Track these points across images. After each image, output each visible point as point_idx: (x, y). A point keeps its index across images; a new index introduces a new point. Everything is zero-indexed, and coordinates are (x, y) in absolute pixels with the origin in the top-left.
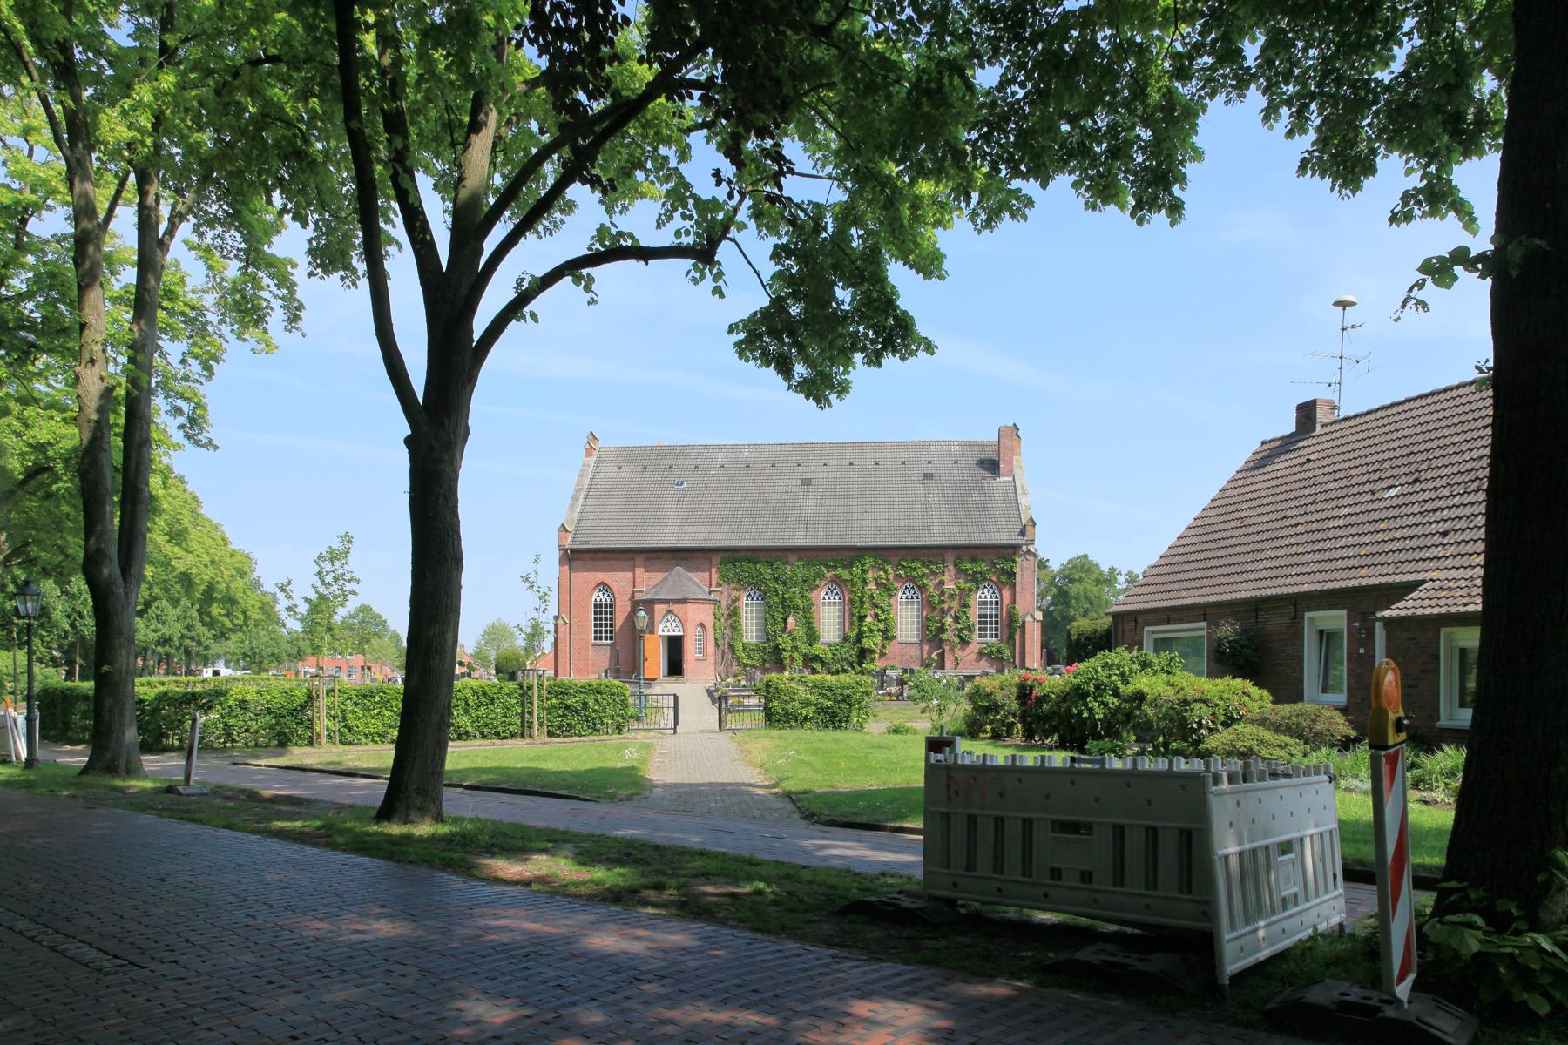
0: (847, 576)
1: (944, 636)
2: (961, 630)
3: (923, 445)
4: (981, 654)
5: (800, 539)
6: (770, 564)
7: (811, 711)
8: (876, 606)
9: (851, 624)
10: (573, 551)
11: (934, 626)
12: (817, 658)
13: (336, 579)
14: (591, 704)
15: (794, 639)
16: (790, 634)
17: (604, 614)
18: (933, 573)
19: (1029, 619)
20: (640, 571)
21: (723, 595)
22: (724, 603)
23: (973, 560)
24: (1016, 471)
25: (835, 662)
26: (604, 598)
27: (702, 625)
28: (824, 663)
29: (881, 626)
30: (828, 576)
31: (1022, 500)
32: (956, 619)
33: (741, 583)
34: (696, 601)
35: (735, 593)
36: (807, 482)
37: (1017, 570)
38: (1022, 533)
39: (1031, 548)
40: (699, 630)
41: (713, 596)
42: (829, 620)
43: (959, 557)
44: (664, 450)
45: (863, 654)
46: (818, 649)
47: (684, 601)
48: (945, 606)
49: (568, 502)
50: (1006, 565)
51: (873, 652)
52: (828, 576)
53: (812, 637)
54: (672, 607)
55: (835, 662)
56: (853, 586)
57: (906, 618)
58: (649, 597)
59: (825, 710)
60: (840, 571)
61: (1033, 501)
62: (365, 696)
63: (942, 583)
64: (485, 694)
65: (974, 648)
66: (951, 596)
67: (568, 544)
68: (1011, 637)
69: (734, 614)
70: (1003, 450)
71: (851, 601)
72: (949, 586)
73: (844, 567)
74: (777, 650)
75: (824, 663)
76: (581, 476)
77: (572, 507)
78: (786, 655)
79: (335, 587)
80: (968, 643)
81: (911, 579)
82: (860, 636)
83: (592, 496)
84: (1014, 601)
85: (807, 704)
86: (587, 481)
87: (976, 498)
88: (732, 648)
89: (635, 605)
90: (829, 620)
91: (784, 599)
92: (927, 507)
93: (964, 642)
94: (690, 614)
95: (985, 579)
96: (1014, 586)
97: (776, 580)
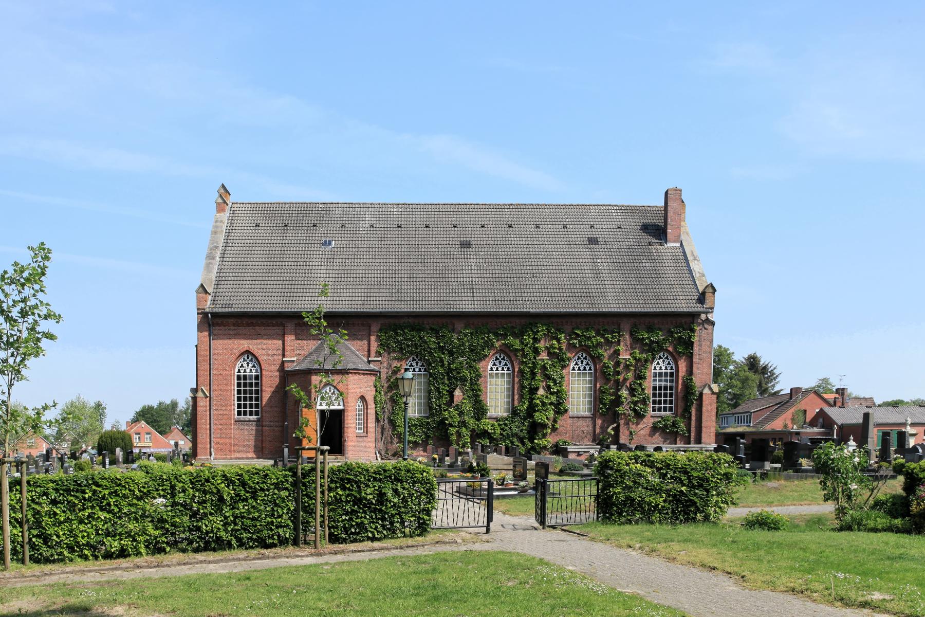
0: (517, 344)
1: (620, 409)
2: (635, 403)
3: (583, 208)
4: (655, 428)
5: (468, 304)
6: (435, 332)
7: (660, 500)
8: (548, 377)
9: (521, 397)
10: (215, 315)
11: (608, 398)
12: (485, 434)
13: (24, 314)
14: (390, 494)
15: (461, 414)
16: (457, 408)
17: (248, 388)
18: (608, 343)
19: (706, 391)
20: (290, 339)
21: (384, 365)
22: (384, 374)
23: (650, 329)
24: (683, 237)
25: (504, 438)
26: (250, 370)
27: (363, 398)
28: (492, 439)
29: (554, 399)
30: (497, 345)
31: (694, 266)
32: (632, 391)
33: (402, 352)
34: (357, 372)
35: (396, 364)
36: (466, 245)
37: (695, 339)
38: (702, 299)
39: (710, 316)
40: (360, 404)
41: (372, 366)
42: (497, 394)
43: (635, 326)
44: (305, 209)
45: (535, 429)
46: (487, 424)
47: (344, 372)
48: (621, 378)
49: (203, 262)
50: (684, 334)
51: (545, 426)
52: (497, 345)
53: (480, 410)
54: (331, 377)
55: (504, 438)
56: (524, 356)
57: (578, 391)
58: (303, 366)
59: (676, 498)
60: (510, 340)
61: (705, 269)
62: (68, 491)
63: (617, 353)
64: (244, 484)
65: (648, 422)
66: (627, 367)
67: (208, 306)
68: (687, 410)
69: (394, 385)
70: (671, 213)
71: (521, 372)
72: (625, 356)
73: (515, 336)
74: (443, 426)
75: (492, 439)
76: (215, 233)
77: (208, 266)
78: (453, 430)
79: (24, 327)
80: (644, 416)
81: (585, 349)
82: (532, 409)
83: (230, 254)
84: (690, 372)
85: (657, 490)
86: (221, 239)
87: (646, 264)
88: (392, 423)
89: (286, 376)
90: (497, 394)
91: (450, 370)
92: (597, 273)
93: (639, 416)
94: (351, 386)
95: (662, 349)
96: (690, 357)
97: (441, 349)
